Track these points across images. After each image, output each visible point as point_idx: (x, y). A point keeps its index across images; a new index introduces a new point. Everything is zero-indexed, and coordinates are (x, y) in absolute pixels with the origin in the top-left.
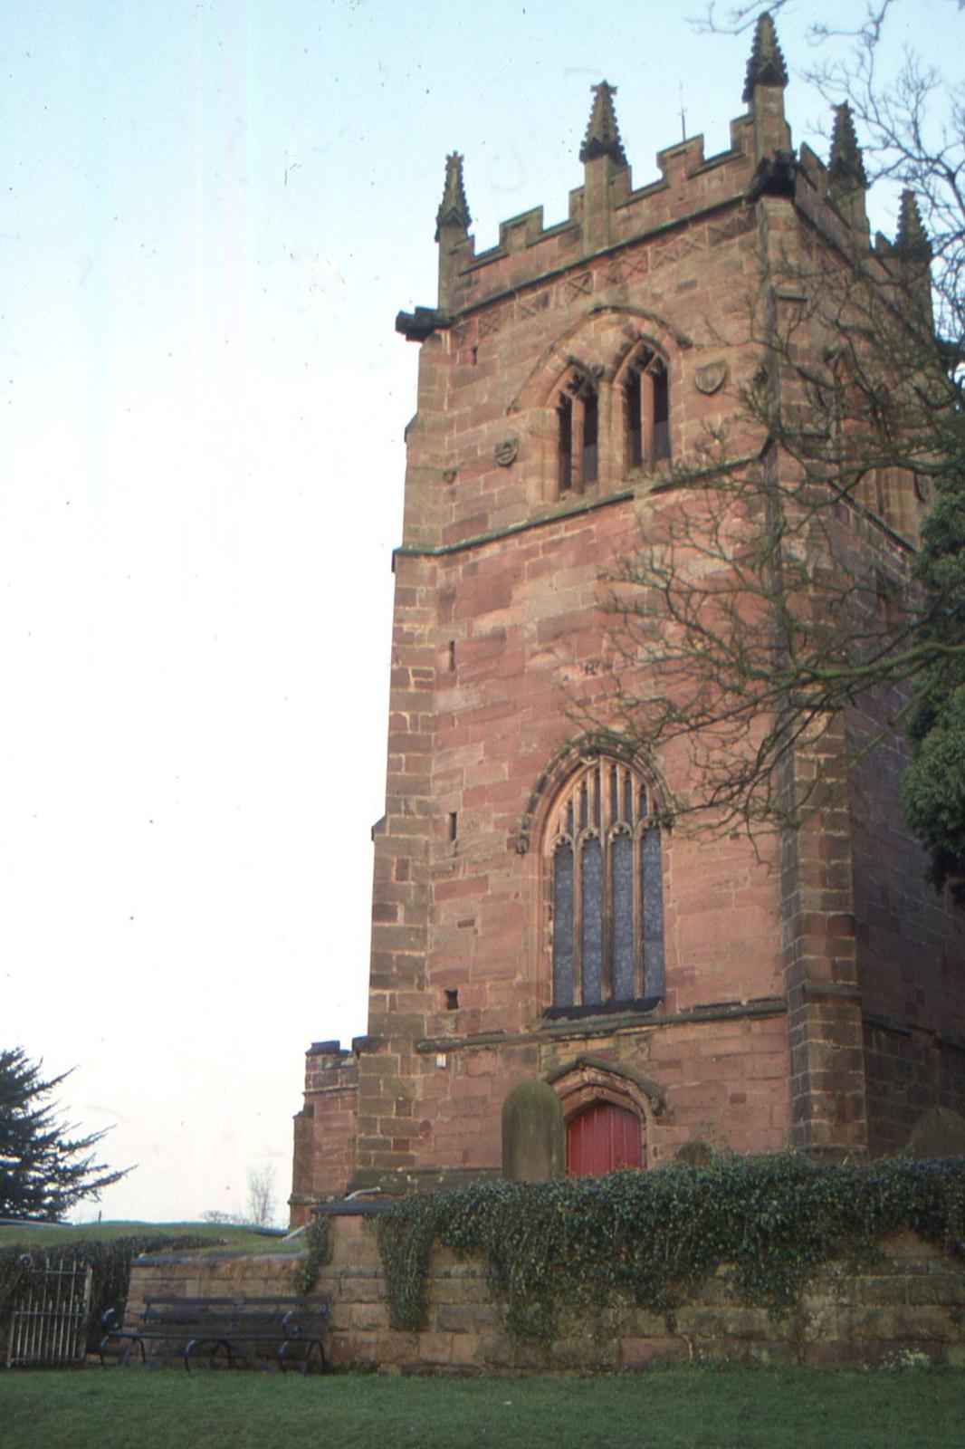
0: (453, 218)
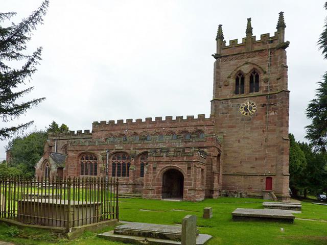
0: (220, 37)
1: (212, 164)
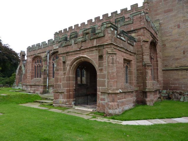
1: (142, 54)
